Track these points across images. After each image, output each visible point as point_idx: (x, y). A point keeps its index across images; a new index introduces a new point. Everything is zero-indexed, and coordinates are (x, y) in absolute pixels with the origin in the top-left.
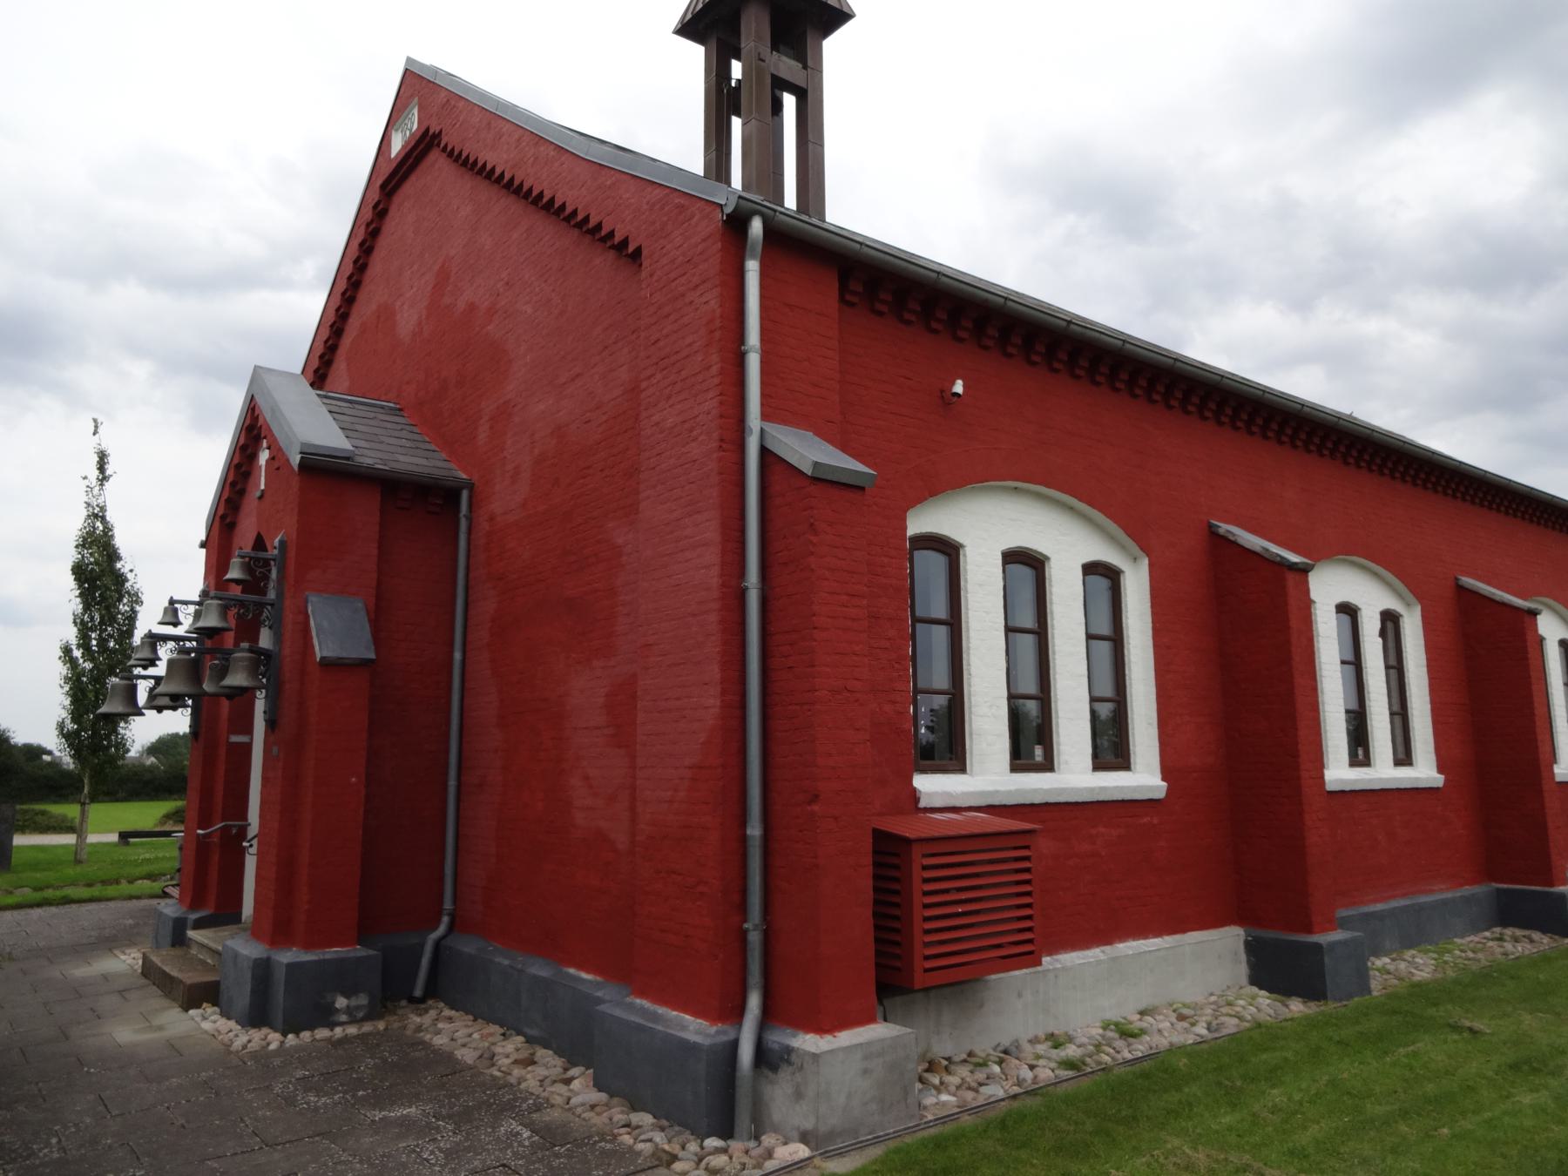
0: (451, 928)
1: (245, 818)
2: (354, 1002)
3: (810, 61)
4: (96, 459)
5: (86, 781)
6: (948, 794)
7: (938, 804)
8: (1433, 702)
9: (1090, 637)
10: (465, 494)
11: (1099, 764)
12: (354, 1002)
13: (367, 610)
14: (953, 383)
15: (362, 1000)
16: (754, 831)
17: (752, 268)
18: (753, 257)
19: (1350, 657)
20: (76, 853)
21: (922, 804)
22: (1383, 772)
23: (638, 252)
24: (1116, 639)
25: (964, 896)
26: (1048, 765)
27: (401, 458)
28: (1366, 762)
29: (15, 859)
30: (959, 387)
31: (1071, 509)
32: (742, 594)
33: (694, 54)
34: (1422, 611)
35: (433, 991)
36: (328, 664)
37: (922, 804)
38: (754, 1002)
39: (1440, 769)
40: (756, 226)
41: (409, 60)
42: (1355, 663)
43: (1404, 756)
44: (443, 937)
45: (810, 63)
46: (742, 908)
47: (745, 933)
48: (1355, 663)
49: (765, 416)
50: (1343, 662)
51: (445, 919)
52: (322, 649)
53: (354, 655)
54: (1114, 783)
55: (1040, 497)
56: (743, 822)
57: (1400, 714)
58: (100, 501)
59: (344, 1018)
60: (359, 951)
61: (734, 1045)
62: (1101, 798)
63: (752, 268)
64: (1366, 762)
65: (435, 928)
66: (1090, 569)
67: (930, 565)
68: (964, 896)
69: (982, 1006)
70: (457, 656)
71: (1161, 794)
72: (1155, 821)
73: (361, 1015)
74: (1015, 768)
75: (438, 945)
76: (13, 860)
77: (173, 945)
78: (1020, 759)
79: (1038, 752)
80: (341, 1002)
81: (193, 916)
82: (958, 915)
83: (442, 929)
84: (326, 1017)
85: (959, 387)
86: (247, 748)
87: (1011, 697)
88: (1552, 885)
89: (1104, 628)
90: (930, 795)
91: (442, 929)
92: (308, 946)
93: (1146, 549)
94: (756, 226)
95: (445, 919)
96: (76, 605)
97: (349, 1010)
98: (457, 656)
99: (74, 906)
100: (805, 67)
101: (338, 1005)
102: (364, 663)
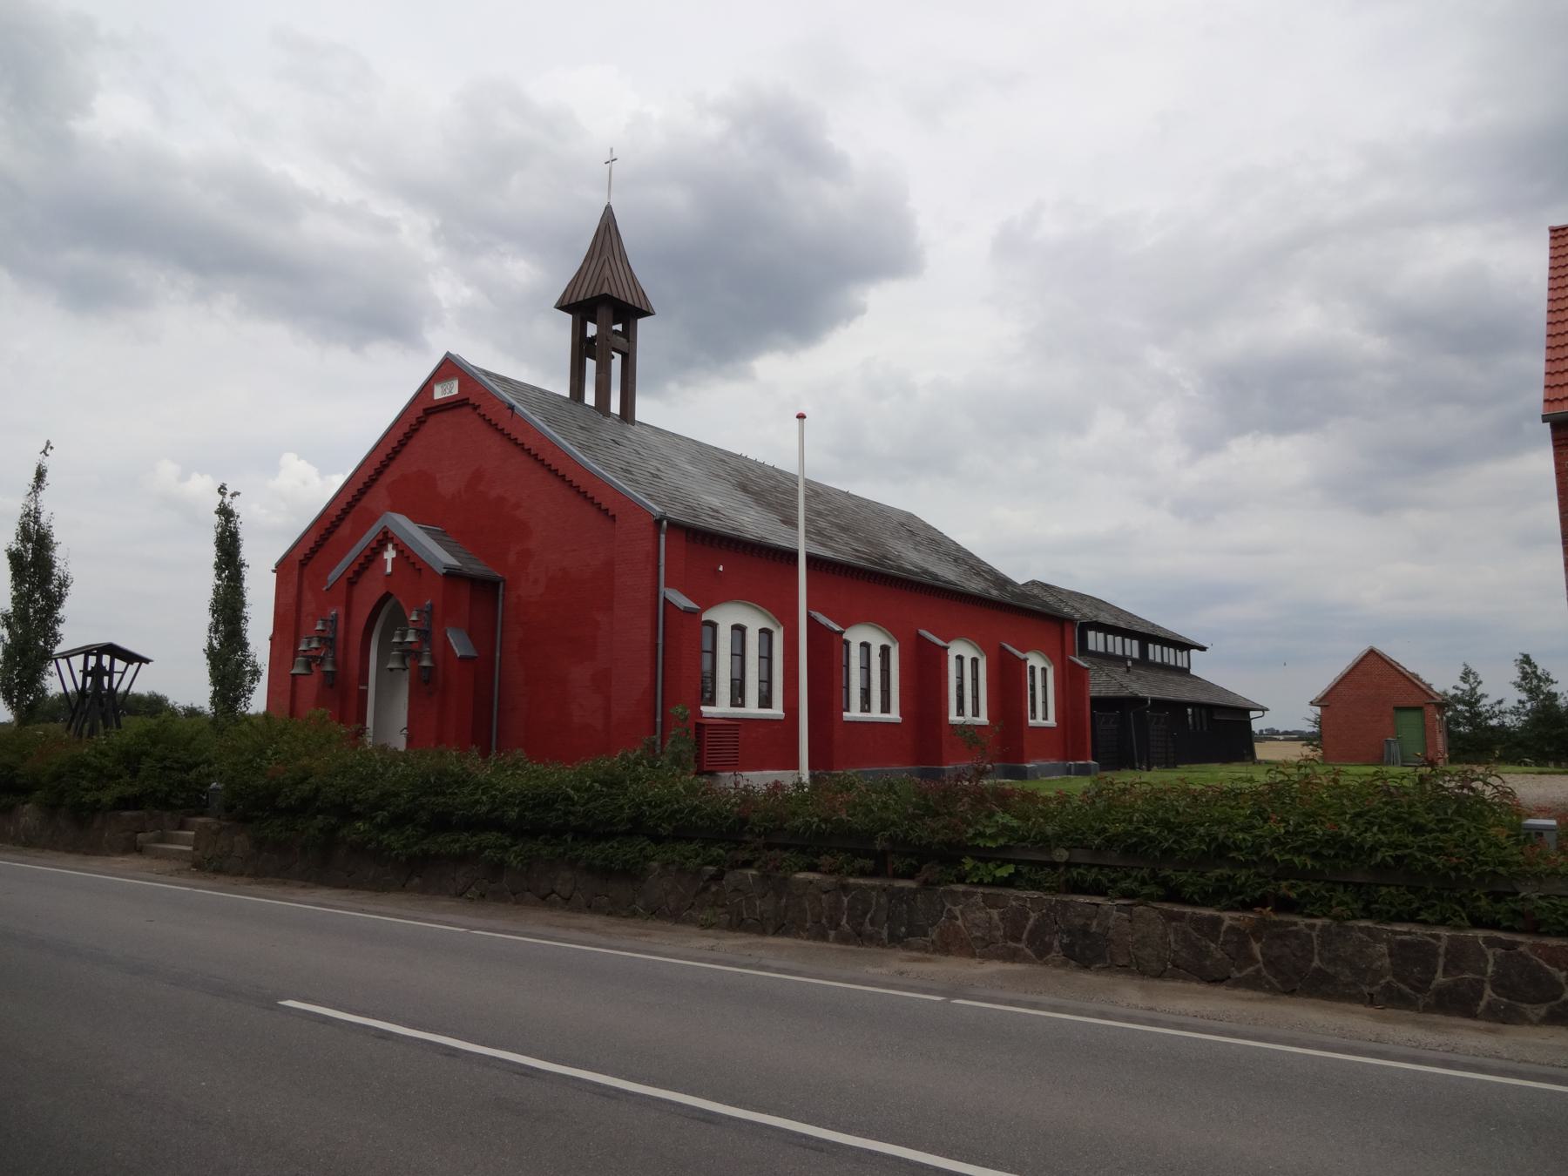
1: (364, 724)
3: (629, 334)
7: (708, 716)
8: (900, 686)
9: (760, 657)
10: (501, 585)
16: (659, 720)
17: (663, 536)
19: (864, 665)
22: (876, 714)
23: (614, 516)
24: (770, 659)
26: (742, 705)
28: (869, 711)
30: (721, 569)
31: (756, 608)
36: (462, 658)
39: (901, 715)
40: (665, 523)
41: (448, 353)
42: (866, 668)
43: (886, 708)
45: (631, 339)
48: (866, 668)
49: (665, 586)
50: (861, 667)
54: (766, 712)
55: (744, 604)
56: (655, 717)
57: (976, 697)
63: (663, 536)
64: (869, 711)
66: (762, 631)
67: (707, 630)
71: (782, 718)
74: (732, 706)
78: (883, 711)
79: (740, 700)
85: (721, 569)
86: (365, 692)
87: (732, 680)
89: (765, 655)
90: (707, 713)
93: (782, 624)
94: (665, 523)
98: (498, 654)
100: (628, 341)
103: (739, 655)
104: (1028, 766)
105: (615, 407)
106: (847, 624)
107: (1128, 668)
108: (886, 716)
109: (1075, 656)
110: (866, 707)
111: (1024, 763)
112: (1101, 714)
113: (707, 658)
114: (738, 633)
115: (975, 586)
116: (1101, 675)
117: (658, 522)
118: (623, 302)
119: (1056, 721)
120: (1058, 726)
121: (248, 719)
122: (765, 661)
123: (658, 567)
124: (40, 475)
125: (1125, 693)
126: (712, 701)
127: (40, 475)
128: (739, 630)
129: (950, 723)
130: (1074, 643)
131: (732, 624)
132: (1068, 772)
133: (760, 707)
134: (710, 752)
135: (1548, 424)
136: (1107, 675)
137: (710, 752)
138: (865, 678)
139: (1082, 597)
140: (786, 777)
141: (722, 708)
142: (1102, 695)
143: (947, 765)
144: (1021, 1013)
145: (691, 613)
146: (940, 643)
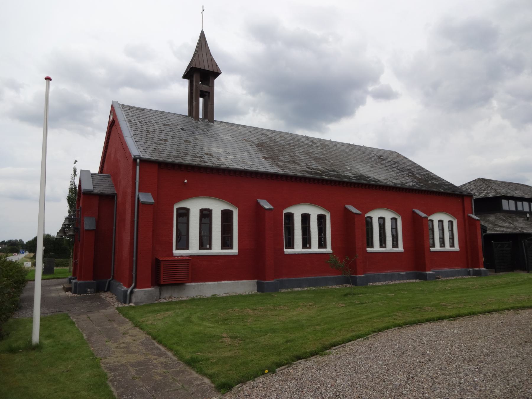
0: (113, 279)
2: (91, 290)
4: (73, 170)
5: (71, 252)
6: (180, 254)
10: (116, 196)
11: (451, 247)
12: (91, 290)
13: (96, 220)
14: (185, 180)
15: (93, 290)
16: (134, 259)
17: (138, 167)
18: (138, 166)
19: (441, 229)
20: (69, 270)
21: (174, 255)
25: (172, 270)
27: (104, 189)
29: (55, 271)
30: (186, 181)
32: (134, 221)
33: (186, 82)
34: (331, 214)
35: (108, 290)
37: (174, 255)
38: (133, 285)
40: (138, 160)
43: (322, 244)
44: (111, 280)
45: (211, 85)
46: (132, 271)
47: (132, 274)
51: (112, 277)
52: (86, 227)
53: (92, 229)
58: (74, 181)
59: (89, 293)
60: (93, 281)
61: (127, 291)
62: (220, 254)
63: (138, 167)
65: (110, 278)
68: (172, 270)
69: (184, 289)
70: (114, 228)
72: (235, 259)
73: (92, 292)
75: (110, 282)
76: (54, 272)
77: (69, 283)
78: (381, 246)
80: (89, 290)
81: (73, 278)
82: (171, 273)
83: (111, 279)
84: (86, 292)
85: (186, 181)
88: (356, 275)
90: (176, 253)
91: (111, 279)
92: (83, 280)
94: (138, 160)
95: (112, 277)
96: (68, 208)
97: (90, 291)
98: (114, 228)
99: (60, 279)
101: (88, 290)
102: (94, 230)
103: (442, 230)
104: (428, 273)
106: (430, 213)
107: (528, 218)
108: (323, 250)
109: (472, 214)
110: (443, 245)
111: (426, 271)
112: (497, 242)
113: (430, 232)
114: (441, 223)
115: (409, 183)
116: (506, 223)
117: (135, 160)
118: (204, 69)
119: (459, 247)
120: (404, 251)
122: (441, 231)
123: (135, 183)
125: (517, 231)
126: (372, 246)
128: (441, 222)
129: (285, 253)
130: (472, 207)
131: (318, 214)
132: (469, 274)
133: (303, 248)
134: (164, 270)
136: (509, 222)
137: (164, 270)
138: (451, 234)
139: (432, 174)
142: (504, 232)
143: (430, 270)
145: (359, 214)
146: (423, 215)
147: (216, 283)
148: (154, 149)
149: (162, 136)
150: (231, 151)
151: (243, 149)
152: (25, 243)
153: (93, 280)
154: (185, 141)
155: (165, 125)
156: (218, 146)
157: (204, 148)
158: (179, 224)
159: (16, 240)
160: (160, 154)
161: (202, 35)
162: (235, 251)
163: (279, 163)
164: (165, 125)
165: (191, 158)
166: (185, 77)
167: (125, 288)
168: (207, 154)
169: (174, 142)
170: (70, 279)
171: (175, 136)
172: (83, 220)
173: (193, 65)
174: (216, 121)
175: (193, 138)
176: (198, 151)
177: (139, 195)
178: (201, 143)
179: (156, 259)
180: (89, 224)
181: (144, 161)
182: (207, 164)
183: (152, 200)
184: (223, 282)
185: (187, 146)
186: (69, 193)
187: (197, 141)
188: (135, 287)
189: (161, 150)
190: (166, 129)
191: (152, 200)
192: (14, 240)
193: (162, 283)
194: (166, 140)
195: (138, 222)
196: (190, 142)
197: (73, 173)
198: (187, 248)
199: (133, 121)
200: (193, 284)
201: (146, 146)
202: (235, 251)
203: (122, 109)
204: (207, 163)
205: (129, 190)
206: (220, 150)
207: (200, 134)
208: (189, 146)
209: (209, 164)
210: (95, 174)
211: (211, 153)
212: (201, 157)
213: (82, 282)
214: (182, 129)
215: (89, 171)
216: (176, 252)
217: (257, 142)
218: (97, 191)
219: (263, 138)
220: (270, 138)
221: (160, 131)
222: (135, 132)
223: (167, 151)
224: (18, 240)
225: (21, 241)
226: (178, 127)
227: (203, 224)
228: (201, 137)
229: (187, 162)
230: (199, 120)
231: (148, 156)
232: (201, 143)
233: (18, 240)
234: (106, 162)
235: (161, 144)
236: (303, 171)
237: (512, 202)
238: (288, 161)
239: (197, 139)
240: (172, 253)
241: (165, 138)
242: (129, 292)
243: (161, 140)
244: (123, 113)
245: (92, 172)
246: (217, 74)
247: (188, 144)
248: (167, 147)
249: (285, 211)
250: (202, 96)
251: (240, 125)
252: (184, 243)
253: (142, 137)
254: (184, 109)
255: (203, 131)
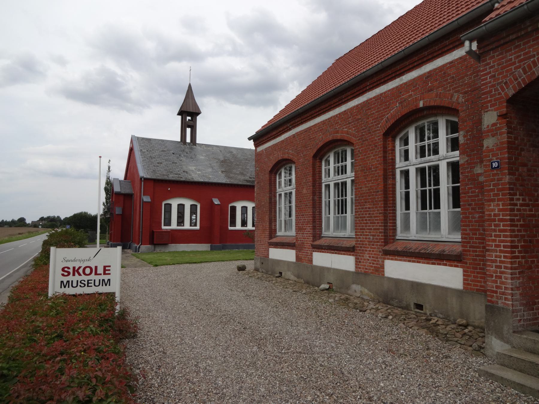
16: (141, 230)
17: (143, 183)
27: (127, 191)
30: (169, 189)
35: (129, 248)
40: (143, 179)
52: (117, 213)
60: (121, 243)
63: (143, 183)
66: (191, 205)
85: (169, 189)
94: (143, 179)
105: (188, 140)
117: (141, 179)
121: (463, 243)
124: (109, 168)
127: (109, 168)
133: (241, 227)
135: (252, 140)
140: (516, 265)
141: (238, 226)
144: (22, 264)
147: (186, 244)
148: (152, 171)
149: (159, 160)
150: (200, 168)
151: (210, 166)
152: (62, 219)
153: (121, 242)
154: (173, 163)
155: (163, 151)
156: (194, 164)
157: (184, 167)
158: (166, 213)
159: (54, 217)
160: (156, 174)
161: (190, 86)
162: (198, 227)
163: (231, 175)
164: (163, 151)
165: (173, 176)
166: (179, 114)
167: (136, 245)
168: (184, 172)
169: (166, 164)
170: (108, 243)
171: (168, 159)
172: (115, 209)
173: (182, 110)
174: (198, 144)
175: (179, 160)
176: (179, 170)
177: (144, 198)
178: (183, 163)
179: (153, 231)
180: (118, 211)
181: (146, 179)
182: (181, 179)
183: (150, 200)
184: (190, 244)
185: (173, 166)
186: (106, 184)
187: (181, 162)
188: (141, 245)
189: (157, 171)
190: (163, 154)
191: (150, 200)
192: (52, 216)
193: (155, 243)
194: (161, 163)
195: (142, 212)
196: (176, 163)
197: (108, 170)
198: (170, 225)
199: (143, 150)
200: (173, 245)
201: (148, 169)
202: (198, 227)
203: (137, 141)
204: (182, 178)
205: (138, 194)
206: (193, 168)
207: (184, 156)
208: (175, 166)
209: (183, 179)
210: (122, 181)
211: (187, 170)
212: (180, 174)
213: (115, 243)
214: (173, 154)
215: (118, 179)
216: (164, 227)
217: (222, 158)
218: (123, 192)
219: (228, 155)
220: (234, 155)
221: (159, 157)
222: (144, 158)
223: (160, 171)
224: (56, 216)
225: (58, 217)
226: (171, 152)
227: (397, 168)
228: (184, 159)
229: (170, 178)
230: (186, 145)
231: (148, 177)
232: (183, 163)
233: (56, 216)
234: (128, 171)
235: (158, 166)
236: (246, 180)
237: (195, 218)
238: (239, 173)
239: (181, 161)
240: (162, 228)
241: (160, 162)
242: (138, 247)
243: (158, 163)
244: (138, 144)
245: (120, 179)
246: (198, 113)
247: (175, 164)
248: (161, 168)
249: (230, 205)
250: (189, 127)
251: (215, 146)
252: (168, 222)
253: (147, 162)
254: (177, 138)
255: (187, 153)
